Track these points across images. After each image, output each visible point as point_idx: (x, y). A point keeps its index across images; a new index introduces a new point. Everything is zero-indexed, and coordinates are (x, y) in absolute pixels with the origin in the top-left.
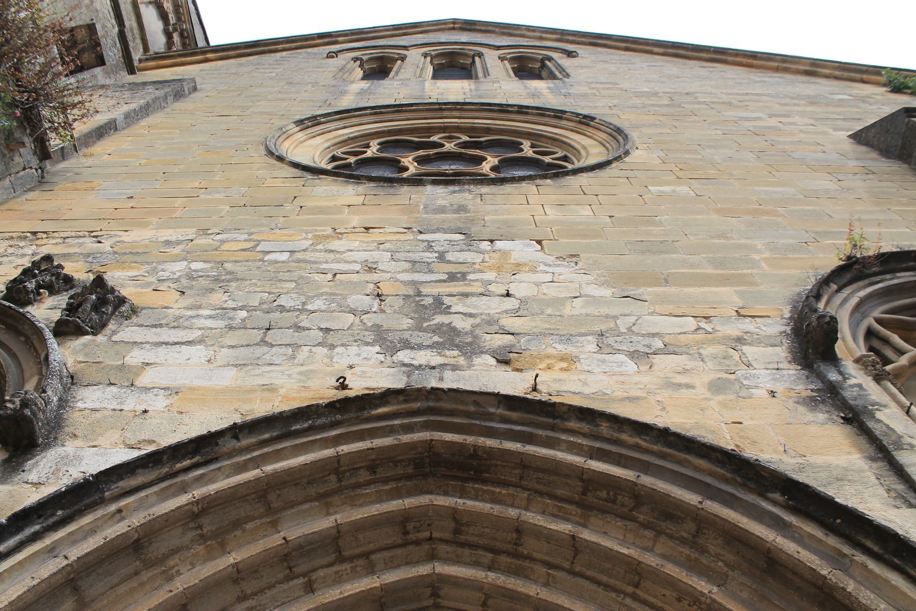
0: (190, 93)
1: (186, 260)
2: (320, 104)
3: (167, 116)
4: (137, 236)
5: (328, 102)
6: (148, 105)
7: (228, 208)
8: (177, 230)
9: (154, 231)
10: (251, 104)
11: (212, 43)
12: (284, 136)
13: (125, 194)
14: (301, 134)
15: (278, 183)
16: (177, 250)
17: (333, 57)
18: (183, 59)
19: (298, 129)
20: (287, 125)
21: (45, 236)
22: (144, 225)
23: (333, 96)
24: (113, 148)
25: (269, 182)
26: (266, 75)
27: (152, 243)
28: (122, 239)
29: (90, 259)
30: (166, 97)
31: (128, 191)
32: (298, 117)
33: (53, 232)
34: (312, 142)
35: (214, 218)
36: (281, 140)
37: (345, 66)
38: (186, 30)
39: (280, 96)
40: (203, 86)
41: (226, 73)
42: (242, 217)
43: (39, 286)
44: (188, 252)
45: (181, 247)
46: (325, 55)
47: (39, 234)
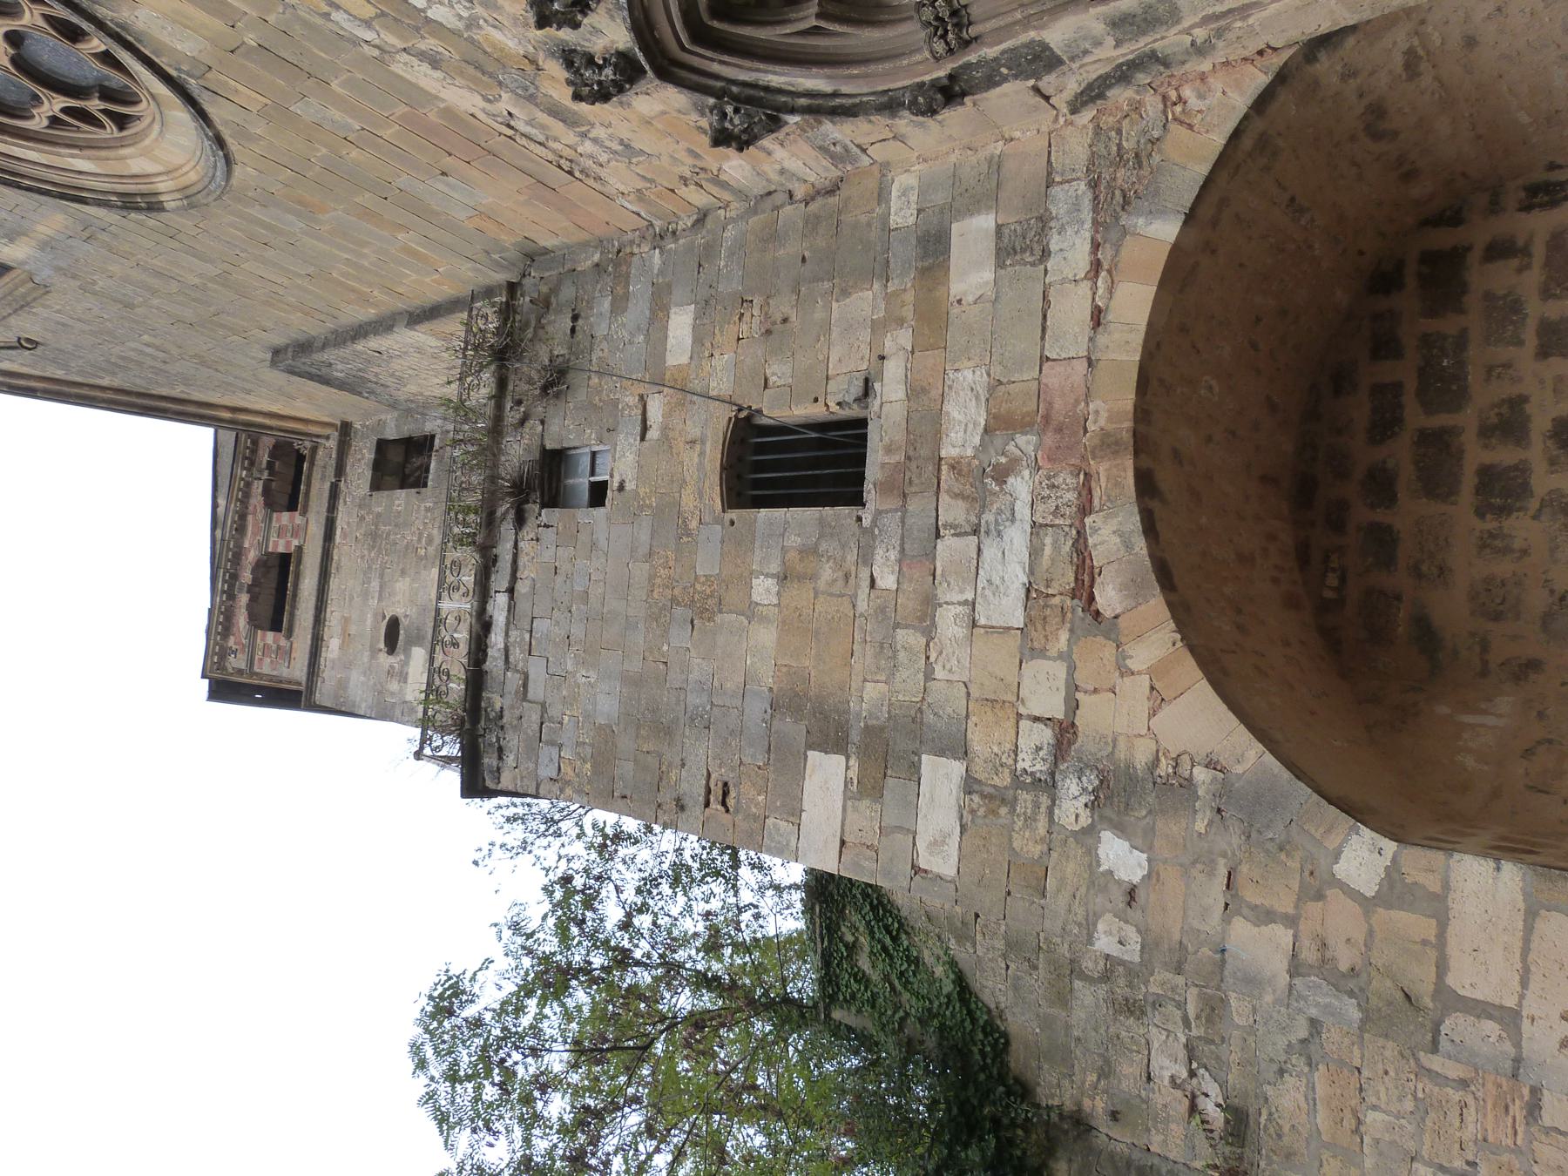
0: (287, 346)
1: (426, 17)
2: (104, 237)
3: (336, 313)
4: (464, 99)
5: (86, 234)
6: (354, 339)
7: (334, 85)
8: (414, 80)
9: (442, 95)
10: (210, 285)
11: (211, 431)
12: (189, 192)
13: (448, 185)
14: (161, 187)
15: (245, 95)
16: (429, 44)
17: (28, 340)
18: (267, 421)
19: (162, 198)
20: (178, 208)
21: (562, 162)
22: (449, 113)
23: (71, 247)
24: (428, 280)
25: (255, 101)
26: (157, 342)
27: (452, 74)
28: (482, 104)
29: (532, 90)
30: (324, 347)
31: (441, 187)
32: (151, 221)
33: (551, 162)
34: (150, 168)
35: (360, 76)
36: (199, 187)
37: (15, 311)
38: (243, 468)
39: (155, 282)
40: (261, 355)
41: (216, 370)
42: (323, 55)
43: (601, 68)
44: (418, 29)
45: (422, 46)
46: (40, 348)
47: (566, 169)
